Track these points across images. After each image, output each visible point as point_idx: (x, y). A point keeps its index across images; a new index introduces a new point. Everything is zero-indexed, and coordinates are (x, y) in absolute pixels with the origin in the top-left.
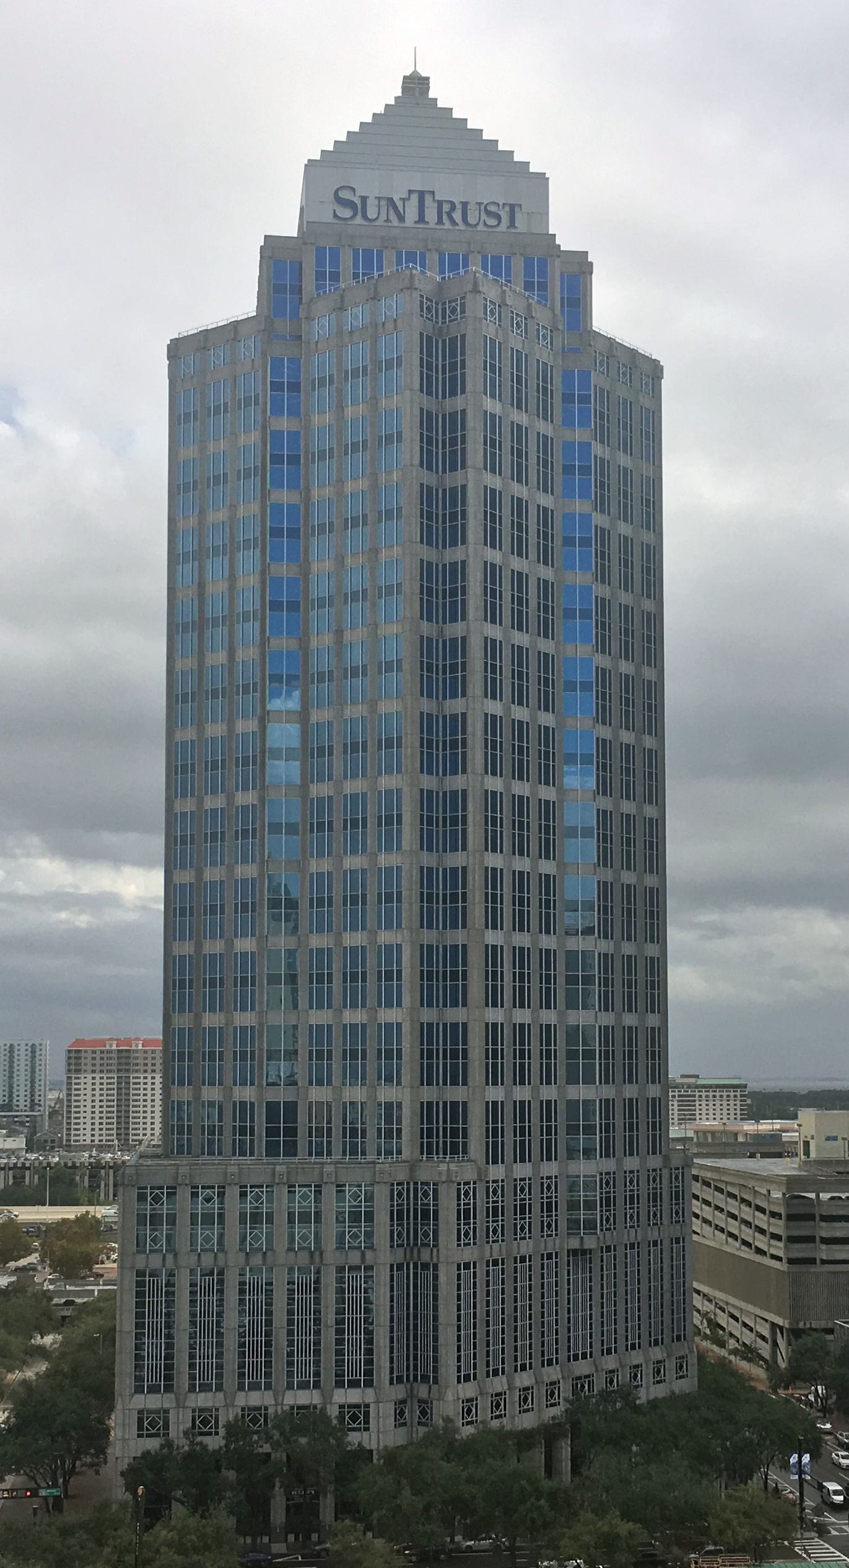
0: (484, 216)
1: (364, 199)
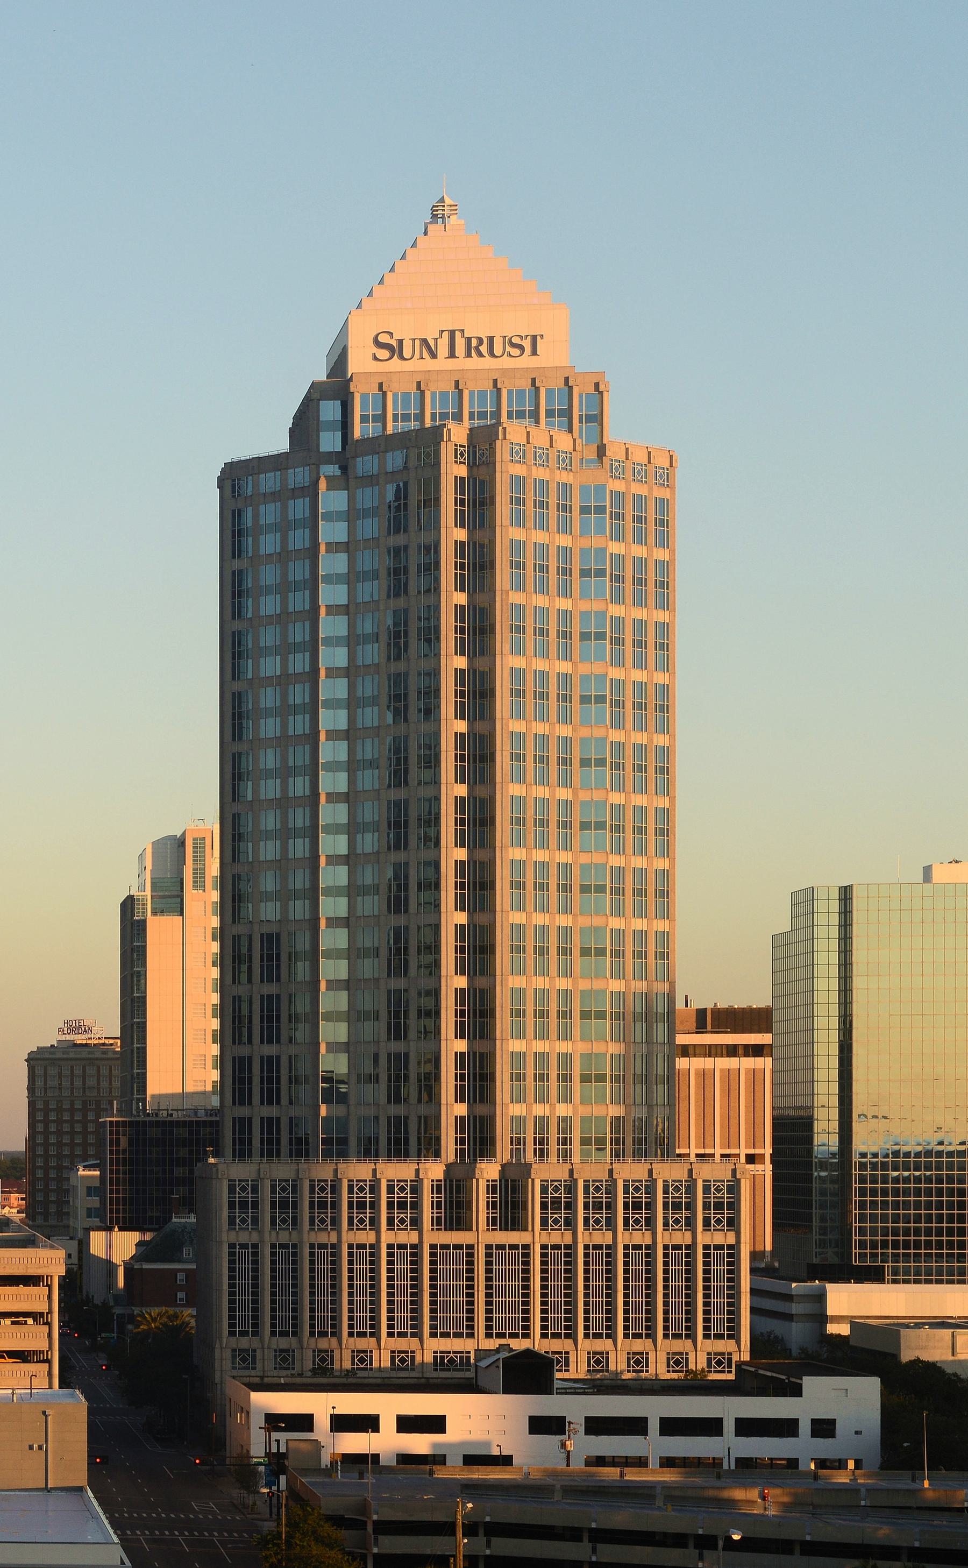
0: (508, 348)
1: (400, 342)
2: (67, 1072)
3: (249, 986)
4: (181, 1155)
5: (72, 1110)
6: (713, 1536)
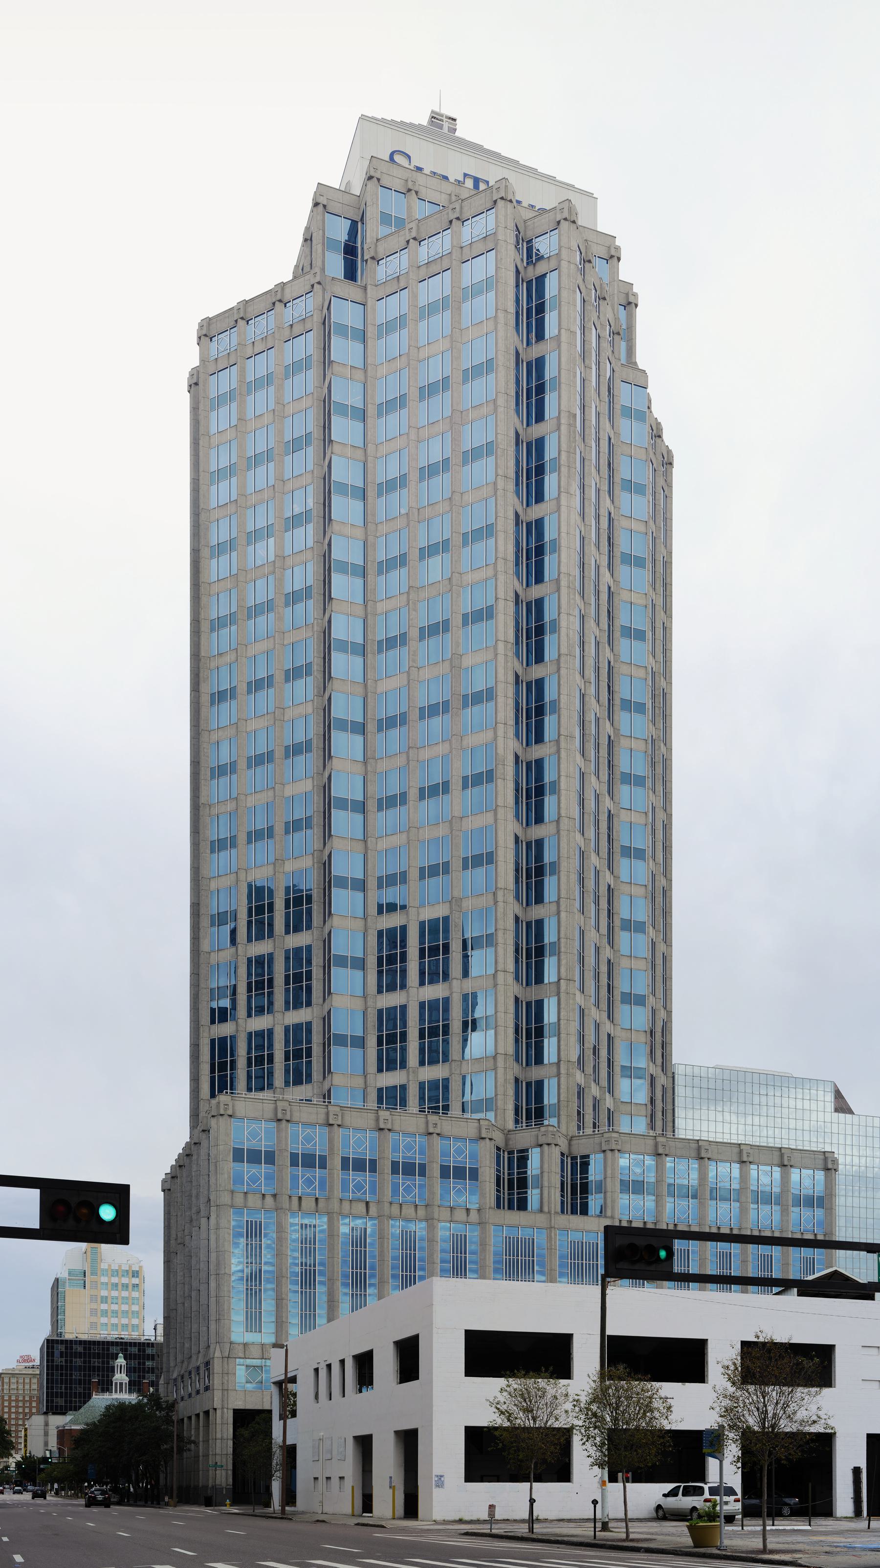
2: (21, 1381)
3: (233, 949)
4: (96, 1364)
5: (24, 1401)
6: (295, 1502)
